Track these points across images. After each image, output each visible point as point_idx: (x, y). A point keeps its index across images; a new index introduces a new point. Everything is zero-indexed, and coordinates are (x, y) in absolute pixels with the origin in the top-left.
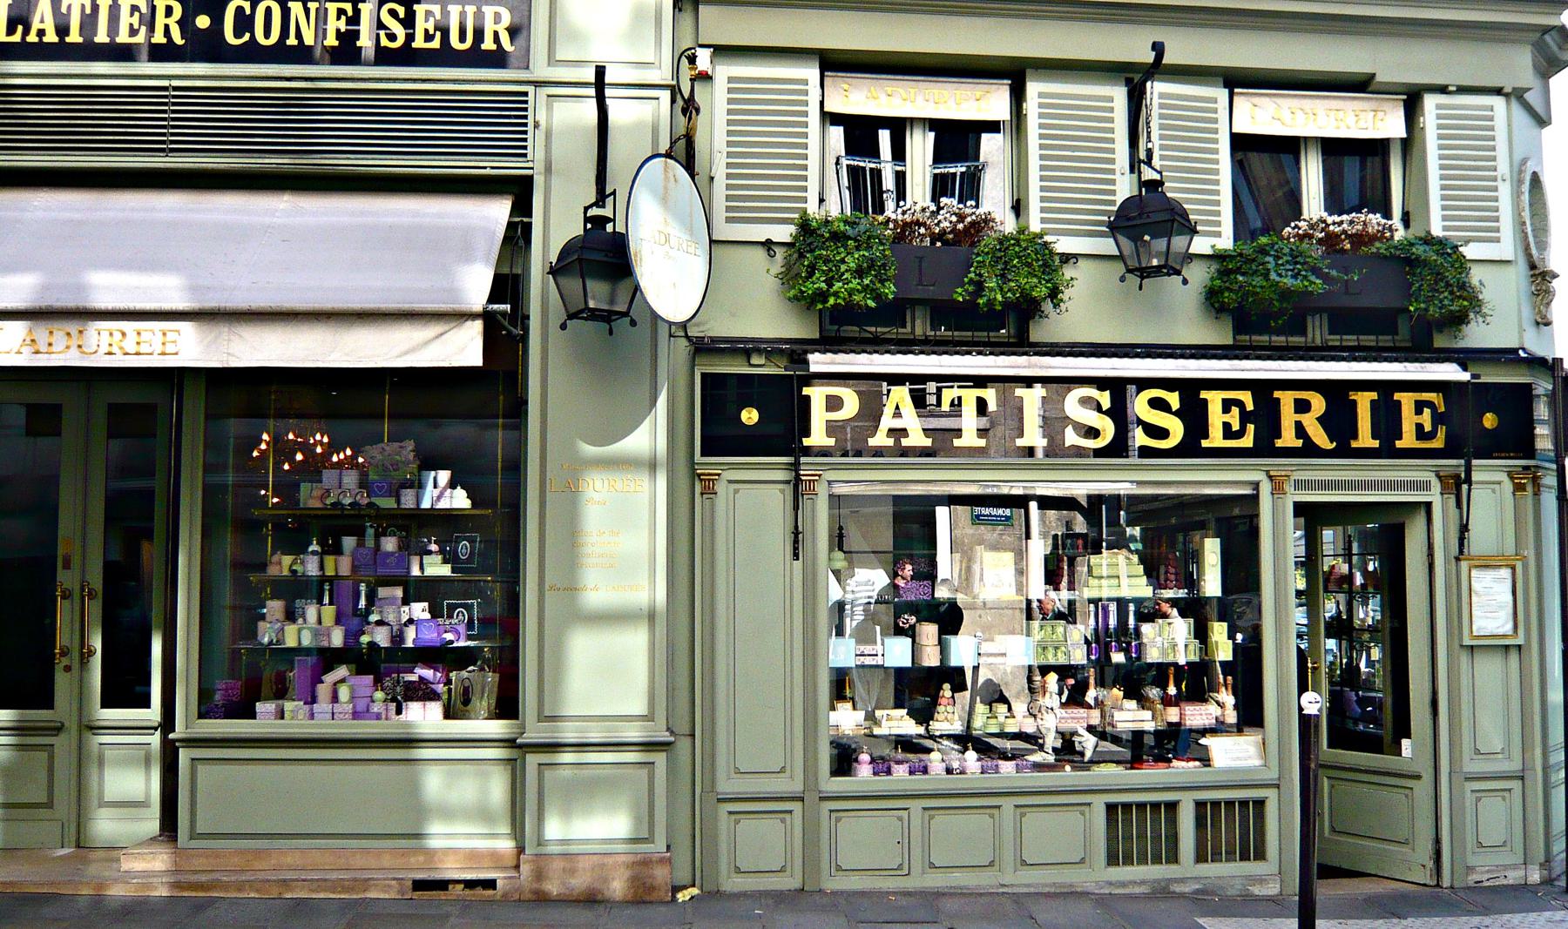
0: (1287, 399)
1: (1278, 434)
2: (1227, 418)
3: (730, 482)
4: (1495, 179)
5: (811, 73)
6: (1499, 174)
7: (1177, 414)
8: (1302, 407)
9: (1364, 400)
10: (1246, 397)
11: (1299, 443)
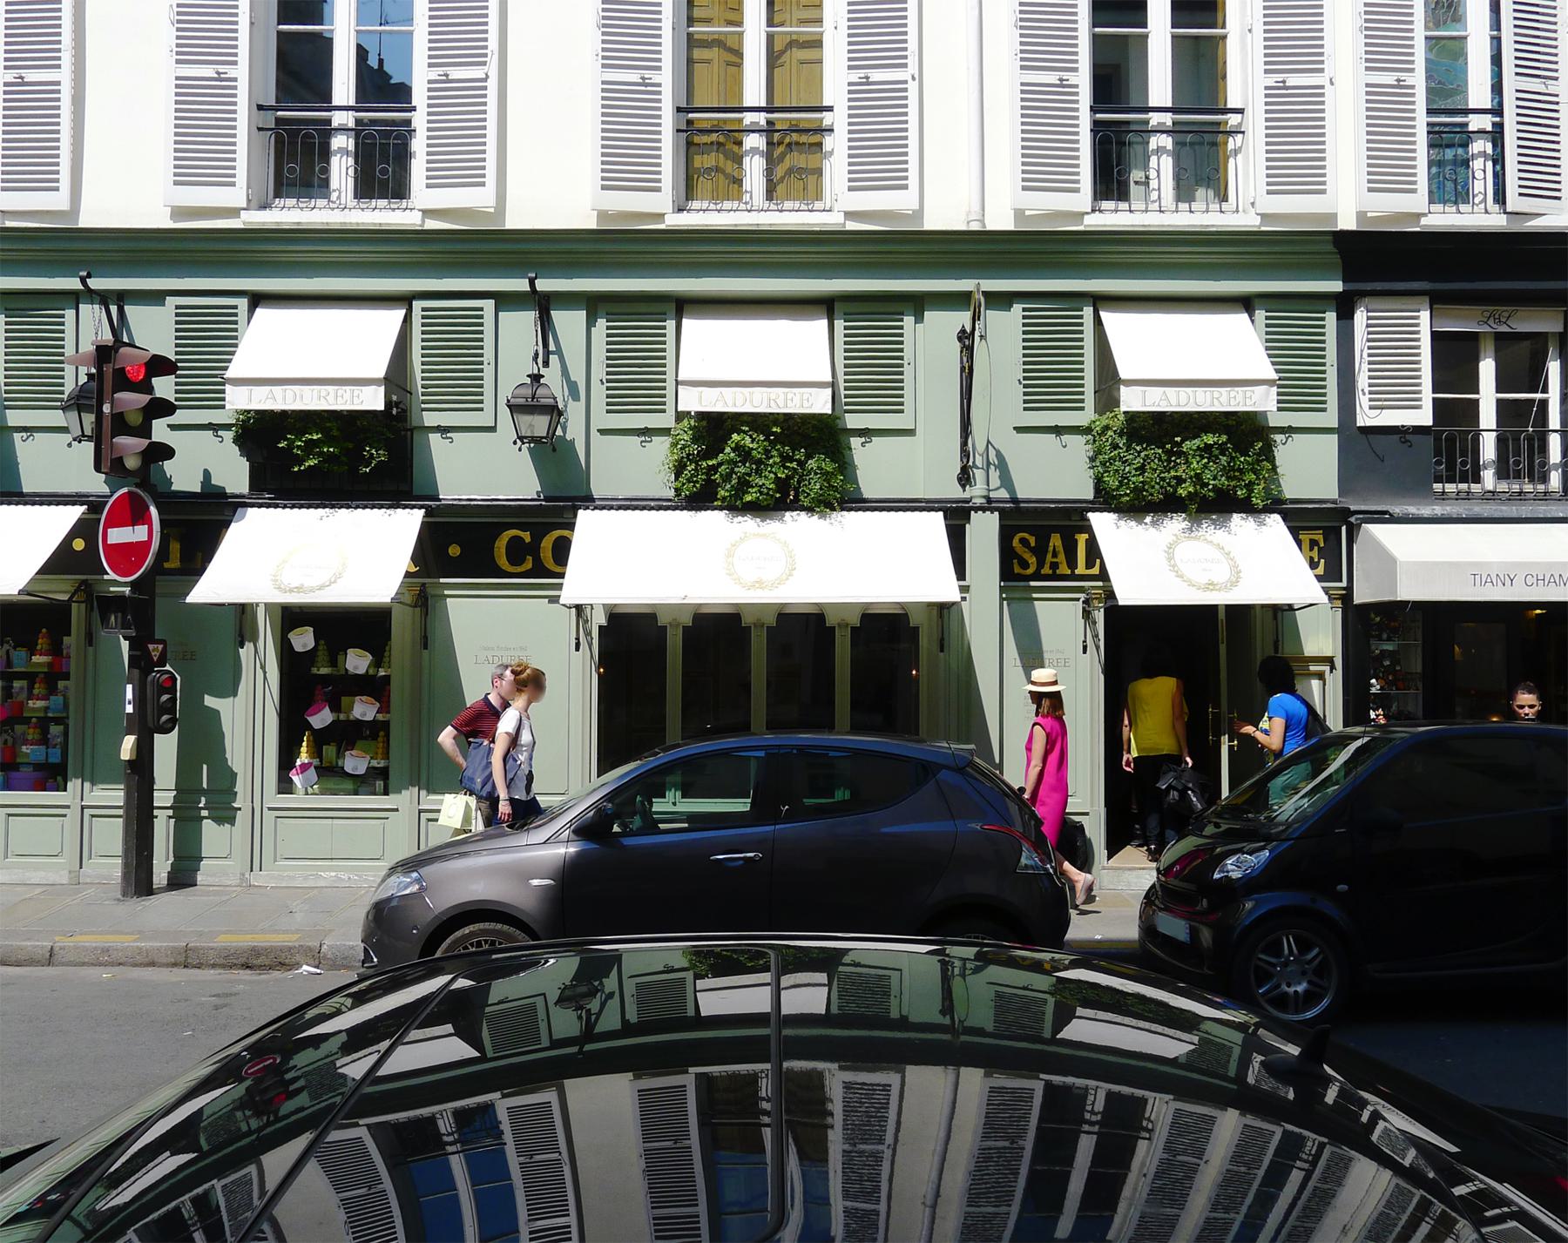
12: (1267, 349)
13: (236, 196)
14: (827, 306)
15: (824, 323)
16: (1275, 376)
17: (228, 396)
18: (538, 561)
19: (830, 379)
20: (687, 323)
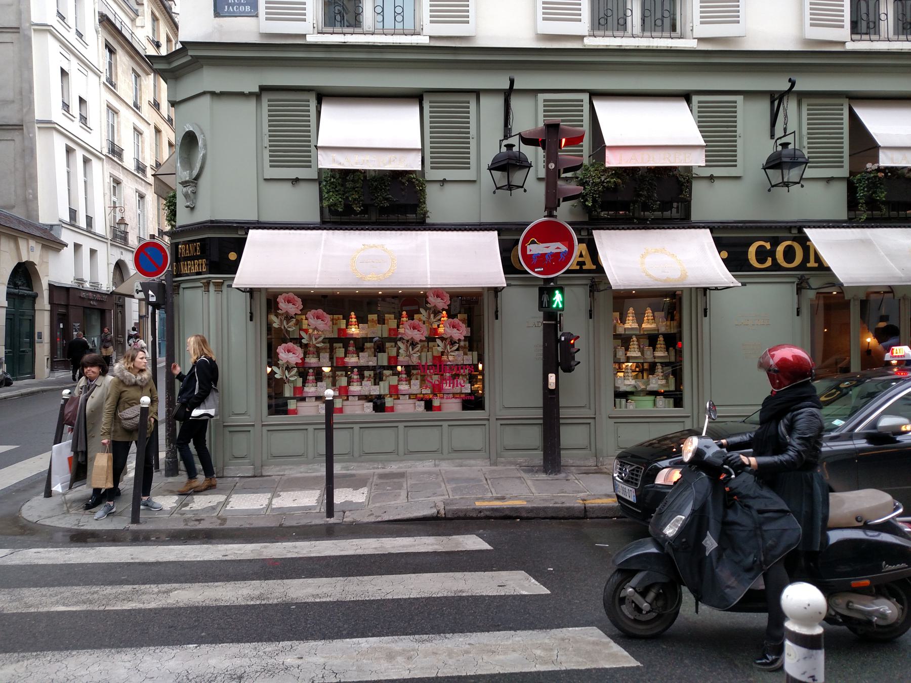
6: (470, 135)
12: (699, 127)
13: (583, 26)
14: (416, 97)
15: (416, 110)
16: (704, 144)
17: (704, 158)
18: (774, 260)
19: (420, 147)
20: (326, 110)
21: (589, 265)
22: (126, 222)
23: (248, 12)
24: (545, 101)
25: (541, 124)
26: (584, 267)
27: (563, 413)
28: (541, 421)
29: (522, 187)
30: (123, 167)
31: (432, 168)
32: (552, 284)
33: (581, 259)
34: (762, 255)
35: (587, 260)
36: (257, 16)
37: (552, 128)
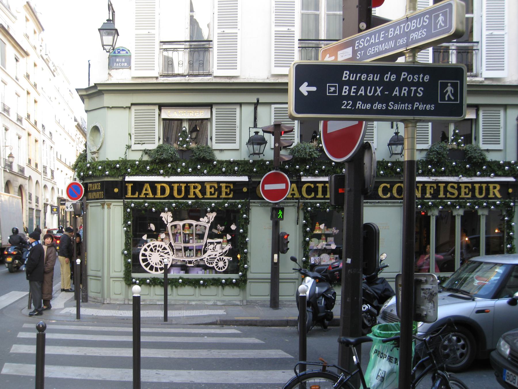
0: (491, 186)
1: (489, 195)
2: (465, 190)
3: (114, 205)
4: (135, 133)
5: (156, 108)
6: (236, 126)
7: (457, 189)
8: (495, 188)
9: (442, 186)
10: (470, 185)
11: (493, 196)
21: (297, 195)
22: (13, 156)
23: (126, 66)
24: (275, 108)
25: (272, 124)
26: (295, 197)
27: (281, 276)
28: (270, 281)
29: (262, 153)
30: (10, 120)
31: (216, 143)
32: (277, 206)
33: (293, 192)
34: (385, 191)
35: (296, 192)
36: (130, 68)
37: (277, 126)
